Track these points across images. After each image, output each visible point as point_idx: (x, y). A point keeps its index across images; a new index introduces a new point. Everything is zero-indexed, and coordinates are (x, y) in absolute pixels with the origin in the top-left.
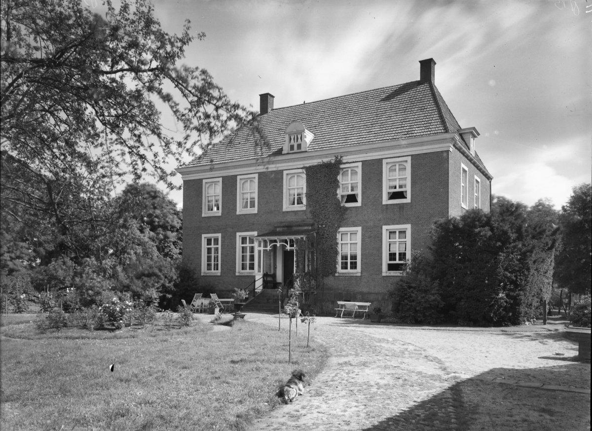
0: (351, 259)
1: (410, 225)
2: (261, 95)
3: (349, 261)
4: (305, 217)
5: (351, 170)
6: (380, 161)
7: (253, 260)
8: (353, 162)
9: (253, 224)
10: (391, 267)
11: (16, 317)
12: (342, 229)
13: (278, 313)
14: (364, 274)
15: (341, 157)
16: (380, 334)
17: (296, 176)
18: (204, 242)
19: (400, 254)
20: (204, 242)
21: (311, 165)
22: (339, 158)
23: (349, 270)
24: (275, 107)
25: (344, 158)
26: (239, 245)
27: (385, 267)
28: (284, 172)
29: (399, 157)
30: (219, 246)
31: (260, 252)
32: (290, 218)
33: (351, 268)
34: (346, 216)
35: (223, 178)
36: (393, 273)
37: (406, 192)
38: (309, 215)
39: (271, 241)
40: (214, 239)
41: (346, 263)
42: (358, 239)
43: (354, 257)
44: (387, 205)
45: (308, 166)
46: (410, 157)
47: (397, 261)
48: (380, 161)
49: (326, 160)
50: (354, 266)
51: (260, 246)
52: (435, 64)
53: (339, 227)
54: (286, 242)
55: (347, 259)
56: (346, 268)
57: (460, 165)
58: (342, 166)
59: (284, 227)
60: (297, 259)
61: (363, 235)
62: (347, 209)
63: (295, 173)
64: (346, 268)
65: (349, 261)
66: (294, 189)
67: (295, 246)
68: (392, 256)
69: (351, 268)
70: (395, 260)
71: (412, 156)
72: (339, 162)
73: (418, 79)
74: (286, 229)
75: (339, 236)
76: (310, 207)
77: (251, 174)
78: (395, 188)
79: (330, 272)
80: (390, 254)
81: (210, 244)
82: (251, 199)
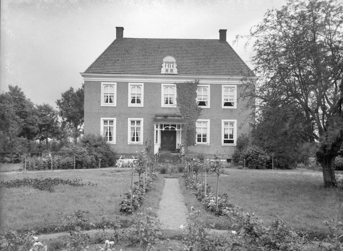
0: (203, 137)
3: (202, 137)
4: (176, 112)
6: (220, 85)
8: (205, 84)
9: (141, 114)
10: (225, 142)
11: (102, 171)
12: (198, 120)
13: (272, 168)
14: (212, 144)
15: (199, 80)
16: (58, 174)
19: (230, 135)
21: (180, 82)
22: (197, 81)
25: (200, 81)
27: (223, 142)
28: (102, 83)
29: (230, 85)
31: (157, 131)
32: (166, 112)
33: (203, 141)
34: (201, 113)
36: (227, 144)
37: (207, 102)
38: (179, 111)
39: (165, 126)
41: (200, 139)
42: (208, 125)
43: (205, 136)
44: (224, 109)
45: (178, 82)
47: (229, 139)
49: (189, 81)
50: (205, 140)
51: (157, 127)
53: (197, 119)
54: (175, 126)
55: (201, 137)
56: (200, 141)
58: (199, 85)
59: (162, 116)
60: (182, 136)
61: (211, 124)
62: (201, 109)
64: (200, 141)
65: (202, 137)
66: (201, 95)
67: (181, 129)
68: (226, 136)
69: (203, 141)
70: (227, 138)
72: (197, 83)
74: (163, 118)
75: (197, 124)
76: (179, 106)
78: (201, 99)
79: (192, 143)
80: (225, 135)
82: (137, 97)
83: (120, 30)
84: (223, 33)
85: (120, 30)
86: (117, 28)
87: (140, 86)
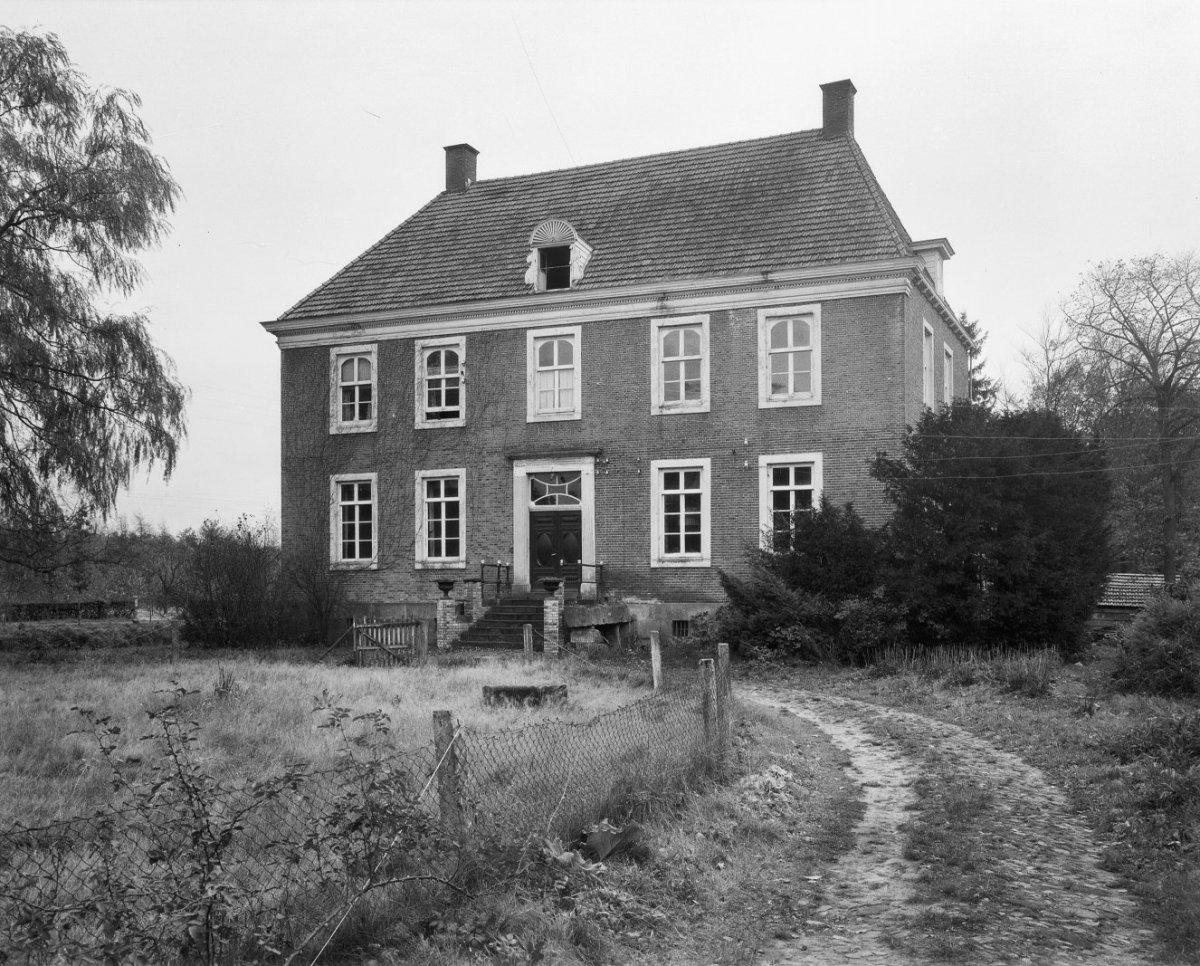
1: (709, 460)
2: (826, 88)
5: (360, 360)
7: (697, 527)
17: (356, 361)
18: (657, 481)
20: (657, 481)
23: (444, 558)
24: (479, 178)
26: (422, 498)
30: (374, 502)
33: (688, 549)
35: (585, 326)
40: (360, 486)
41: (438, 544)
46: (708, 316)
48: (409, 343)
52: (855, 91)
57: (922, 324)
63: (789, 316)
69: (688, 549)
71: (823, 302)
73: (820, 125)
77: (448, 336)
81: (351, 498)
83: (460, 158)
84: (838, 97)
85: (460, 158)
86: (451, 151)
87: (368, 357)
